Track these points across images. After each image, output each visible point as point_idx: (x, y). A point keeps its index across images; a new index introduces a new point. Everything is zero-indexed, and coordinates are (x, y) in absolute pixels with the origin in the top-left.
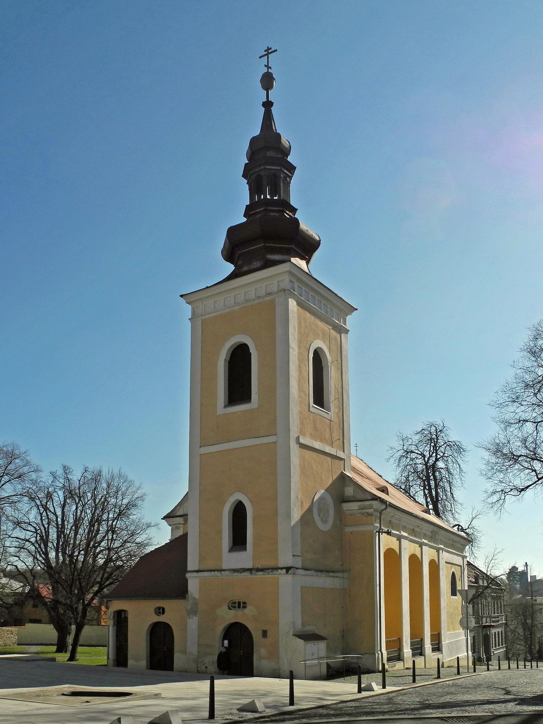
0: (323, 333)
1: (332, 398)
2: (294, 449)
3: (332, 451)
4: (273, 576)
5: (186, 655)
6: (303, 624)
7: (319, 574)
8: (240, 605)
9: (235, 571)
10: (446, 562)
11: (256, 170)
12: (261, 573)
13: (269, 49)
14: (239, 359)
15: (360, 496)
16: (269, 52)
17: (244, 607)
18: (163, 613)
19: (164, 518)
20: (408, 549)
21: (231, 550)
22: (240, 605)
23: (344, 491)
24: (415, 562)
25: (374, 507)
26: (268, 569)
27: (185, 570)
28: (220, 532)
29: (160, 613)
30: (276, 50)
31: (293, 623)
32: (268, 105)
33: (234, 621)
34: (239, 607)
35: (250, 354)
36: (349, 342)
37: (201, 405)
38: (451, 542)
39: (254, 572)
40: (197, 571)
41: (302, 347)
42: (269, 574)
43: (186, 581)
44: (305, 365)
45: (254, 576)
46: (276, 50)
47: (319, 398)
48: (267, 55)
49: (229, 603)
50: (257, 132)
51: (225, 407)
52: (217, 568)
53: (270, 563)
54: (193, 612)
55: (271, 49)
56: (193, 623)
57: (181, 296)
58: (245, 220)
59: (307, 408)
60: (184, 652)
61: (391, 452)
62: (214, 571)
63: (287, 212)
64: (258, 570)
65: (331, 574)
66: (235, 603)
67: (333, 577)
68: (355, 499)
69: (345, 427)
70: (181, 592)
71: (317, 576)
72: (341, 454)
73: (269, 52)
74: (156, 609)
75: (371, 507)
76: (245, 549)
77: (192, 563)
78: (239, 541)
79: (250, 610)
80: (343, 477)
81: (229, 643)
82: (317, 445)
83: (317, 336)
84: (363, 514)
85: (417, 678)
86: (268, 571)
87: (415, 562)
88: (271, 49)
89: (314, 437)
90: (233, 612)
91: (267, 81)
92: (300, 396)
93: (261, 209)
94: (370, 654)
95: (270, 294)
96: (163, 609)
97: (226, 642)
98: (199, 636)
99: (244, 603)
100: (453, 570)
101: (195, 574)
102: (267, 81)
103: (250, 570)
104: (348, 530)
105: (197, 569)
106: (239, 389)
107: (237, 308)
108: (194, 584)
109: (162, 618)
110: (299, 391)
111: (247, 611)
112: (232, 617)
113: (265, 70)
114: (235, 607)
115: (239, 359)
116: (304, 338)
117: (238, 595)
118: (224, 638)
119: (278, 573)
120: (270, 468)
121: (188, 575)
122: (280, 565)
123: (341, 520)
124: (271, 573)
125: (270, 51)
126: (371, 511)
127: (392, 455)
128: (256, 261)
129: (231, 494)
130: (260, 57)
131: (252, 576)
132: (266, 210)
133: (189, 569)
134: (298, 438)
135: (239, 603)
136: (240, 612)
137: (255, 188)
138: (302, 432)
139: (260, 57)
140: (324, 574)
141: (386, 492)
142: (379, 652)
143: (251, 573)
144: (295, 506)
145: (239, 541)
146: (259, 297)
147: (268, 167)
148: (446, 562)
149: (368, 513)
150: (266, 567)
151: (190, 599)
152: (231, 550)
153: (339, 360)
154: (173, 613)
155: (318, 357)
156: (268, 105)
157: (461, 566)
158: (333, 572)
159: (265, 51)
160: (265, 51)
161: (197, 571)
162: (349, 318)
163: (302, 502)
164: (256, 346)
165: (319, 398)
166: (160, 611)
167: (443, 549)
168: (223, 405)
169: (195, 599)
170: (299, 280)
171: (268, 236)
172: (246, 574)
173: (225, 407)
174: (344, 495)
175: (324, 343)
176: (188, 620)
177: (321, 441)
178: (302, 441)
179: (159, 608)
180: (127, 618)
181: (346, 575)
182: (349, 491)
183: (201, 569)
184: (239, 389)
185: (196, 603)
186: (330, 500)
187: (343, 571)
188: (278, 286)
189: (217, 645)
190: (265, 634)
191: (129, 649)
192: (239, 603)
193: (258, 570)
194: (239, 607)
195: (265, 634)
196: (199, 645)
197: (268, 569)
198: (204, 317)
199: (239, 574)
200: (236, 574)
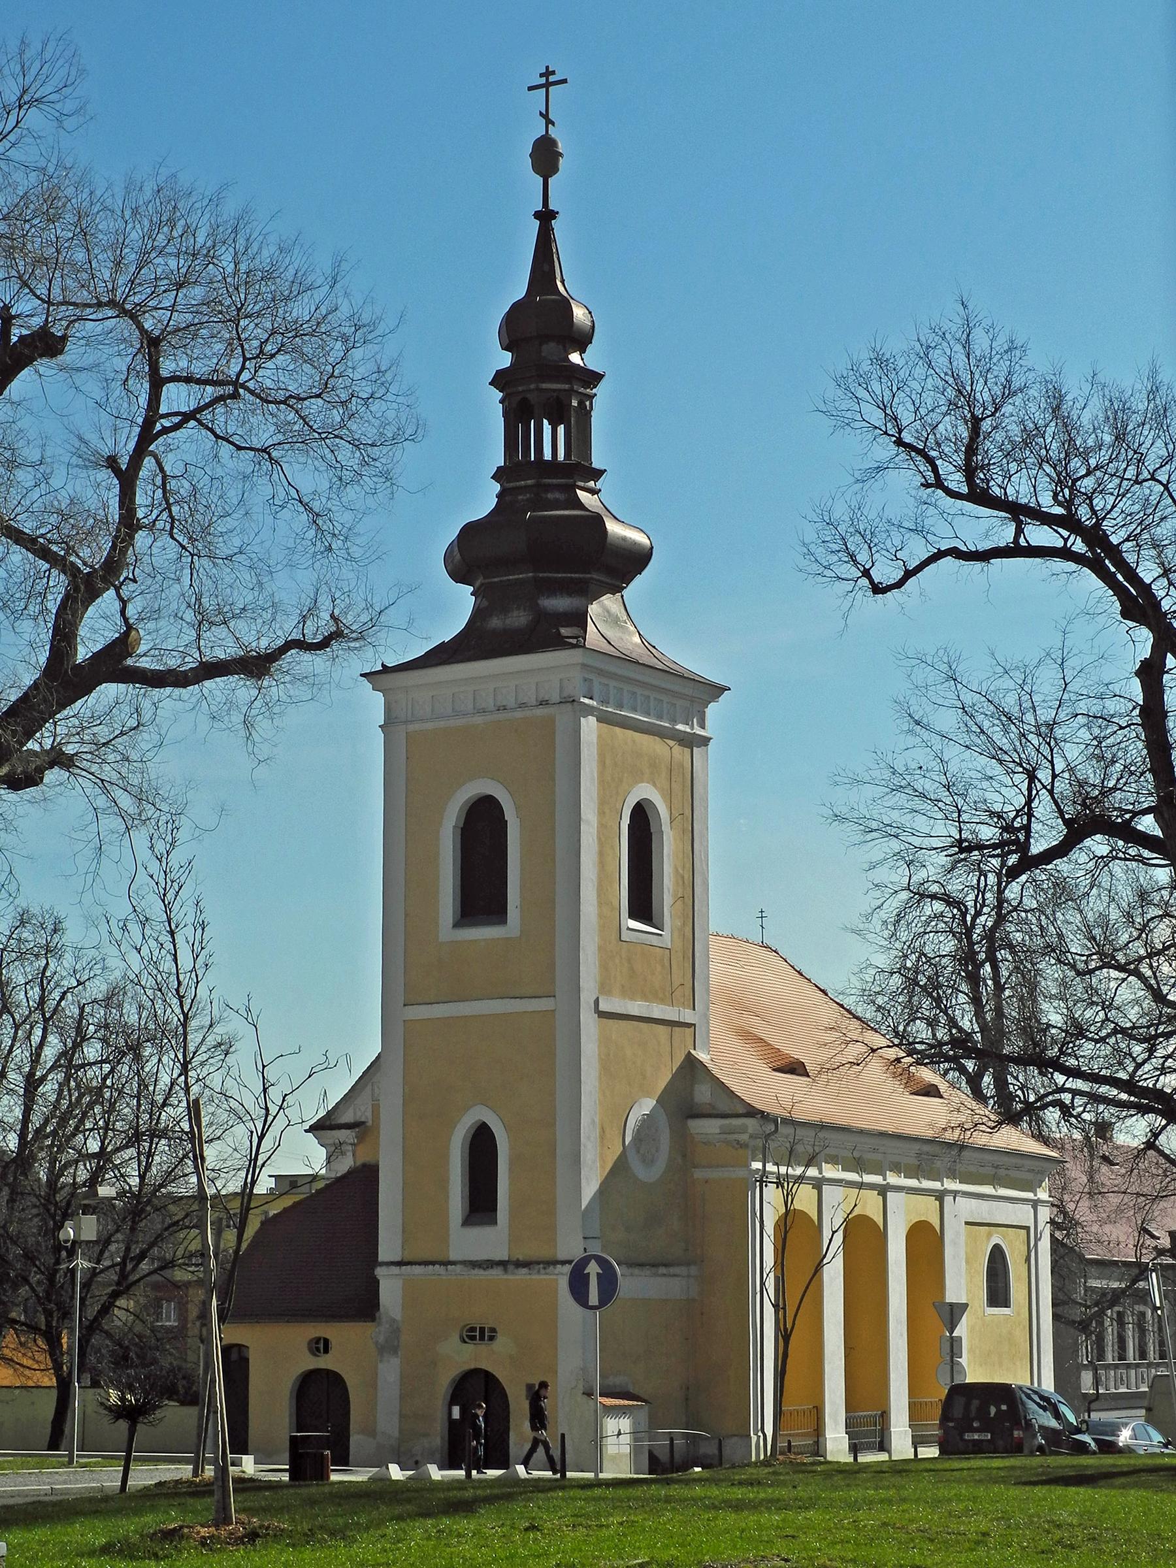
0: (654, 765)
1: (668, 900)
2: (588, 1021)
3: (670, 1013)
4: (548, 1277)
5: (374, 1437)
7: (636, 1271)
8: (477, 1334)
9: (474, 1264)
10: (967, 1223)
11: (520, 389)
12: (525, 1270)
13: (548, 73)
14: (483, 828)
15: (723, 1106)
16: (548, 80)
17: (491, 1338)
18: (326, 1351)
19: (312, 1129)
20: (836, 1208)
21: (467, 1222)
22: (477, 1334)
23: (692, 1096)
24: (864, 1237)
25: (750, 1131)
26: (538, 1263)
27: (371, 1259)
28: (443, 1184)
29: (318, 1349)
30: (564, 81)
31: (584, 1369)
32: (546, 217)
33: (473, 1367)
34: (482, 1338)
36: (712, 766)
37: (406, 915)
38: (991, 1171)
39: (511, 1267)
40: (399, 1264)
41: (607, 811)
42: (539, 1272)
43: (377, 1282)
44: (612, 847)
45: (510, 1277)
46: (564, 81)
47: (642, 905)
48: (547, 85)
49: (462, 1330)
50: (520, 292)
51: (457, 925)
52: (440, 1258)
53: (544, 1253)
54: (389, 1347)
55: (553, 73)
56: (390, 1371)
59: (615, 935)
60: (371, 1432)
61: (878, 894)
62: (433, 1263)
63: (581, 484)
64: (519, 1264)
65: (662, 1270)
66: (473, 1329)
67: (664, 1275)
68: (715, 1112)
69: (697, 954)
70: (365, 1306)
71: (632, 1275)
72: (688, 1016)
73: (548, 80)
74: (311, 1341)
75: (743, 1129)
76: (494, 1222)
77: (388, 1248)
78: (481, 1204)
79: (502, 1344)
80: (691, 1065)
81: (462, 1412)
82: (636, 1007)
83: (637, 776)
84: (727, 1143)
86: (537, 1267)
88: (553, 73)
89: (629, 993)
90: (470, 1348)
91: (545, 157)
92: (601, 916)
93: (529, 482)
94: (741, 1436)
95: (543, 703)
96: (326, 1341)
97: (456, 1412)
98: (402, 1397)
99: (493, 1330)
100: (995, 1240)
101: (395, 1270)
102: (545, 157)
103: (503, 1264)
104: (698, 1174)
105: (398, 1259)
106: (482, 897)
107: (478, 720)
108: (391, 1290)
109: (324, 1362)
110: (600, 904)
112: (465, 1356)
114: (473, 1338)
115: (483, 828)
116: (615, 775)
117: (479, 1315)
118: (452, 1403)
119: (556, 1272)
120: (545, 1055)
121: (380, 1272)
122: (561, 1256)
123: (684, 1156)
124: (542, 1271)
125: (552, 79)
126: (744, 1137)
127: (879, 902)
128: (518, 609)
129: (467, 1108)
130: (530, 89)
131: (505, 1277)
132: (538, 485)
133: (380, 1259)
134: (597, 1002)
135: (482, 1330)
137: (519, 414)
138: (605, 988)
139: (530, 89)
140: (647, 1271)
141: (800, 1071)
142: (760, 1434)
143: (506, 1270)
144: (589, 1138)
145: (481, 1204)
146: (522, 706)
147: (544, 386)
148: (967, 1223)
149: (738, 1142)
150: (534, 1259)
151: (384, 1320)
152: (467, 1222)
153: (688, 812)
154: (349, 1348)
155: (641, 817)
156: (546, 217)
157: (1027, 1228)
158: (665, 1265)
159: (541, 75)
160: (541, 75)
161: (399, 1264)
162: (712, 710)
163: (603, 1130)
164: (518, 808)
165: (642, 905)
166: (321, 1346)
167: (955, 1193)
168: (450, 921)
169: (394, 1320)
170: (601, 673)
171: (541, 559)
172: (496, 1272)
173: (457, 925)
174: (692, 1099)
175: (655, 785)
176: (380, 1366)
177: (645, 998)
178: (603, 1007)
179: (318, 1340)
180: (247, 1360)
181: (694, 1270)
182: (703, 1094)
183: (406, 1260)
184: (482, 897)
185: (396, 1331)
186: (663, 1121)
187: (688, 1264)
188: (561, 688)
189: (439, 1412)
191: (250, 1424)
192: (482, 1330)
193: (519, 1264)
194: (482, 1338)
196: (402, 1416)
197: (538, 1263)
198: (411, 727)
199: (481, 1272)
200: (476, 1271)
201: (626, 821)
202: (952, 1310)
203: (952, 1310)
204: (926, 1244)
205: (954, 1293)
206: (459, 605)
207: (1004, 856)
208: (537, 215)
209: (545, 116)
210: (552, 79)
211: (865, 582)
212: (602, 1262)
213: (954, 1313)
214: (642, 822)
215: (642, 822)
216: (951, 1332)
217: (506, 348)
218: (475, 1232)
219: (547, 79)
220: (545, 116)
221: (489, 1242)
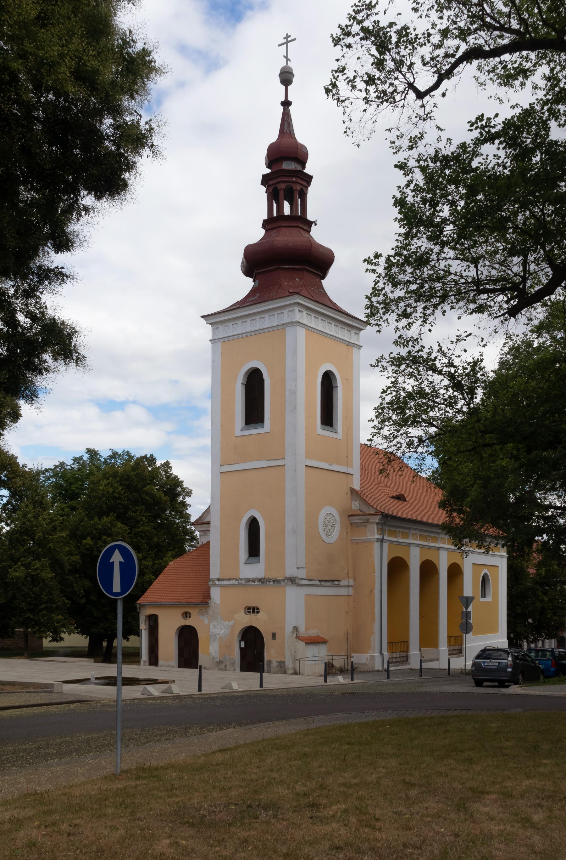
6: (307, 629)
8: (253, 610)
13: (288, 36)
17: (258, 612)
18: (190, 617)
24: (428, 570)
29: (186, 617)
30: (295, 39)
32: (286, 104)
33: (249, 625)
35: (263, 380)
46: (295, 39)
47: (328, 418)
48: (287, 43)
55: (290, 36)
57: (202, 317)
58: (269, 171)
66: (250, 608)
73: (288, 40)
78: (254, 551)
79: (262, 615)
85: (390, 675)
87: (428, 570)
88: (290, 36)
91: (286, 78)
96: (190, 613)
100: (485, 571)
102: (286, 78)
106: (254, 413)
109: (188, 622)
111: (259, 616)
112: (247, 620)
113: (284, 64)
114: (250, 612)
115: (254, 383)
125: (289, 39)
130: (280, 45)
136: (252, 616)
139: (280, 45)
145: (254, 551)
156: (286, 104)
159: (284, 38)
160: (284, 38)
165: (328, 418)
179: (186, 613)
184: (254, 413)
190: (274, 635)
192: (253, 609)
195: (274, 635)
201: (319, 379)
202: (467, 614)
203: (467, 614)
204: (455, 572)
205: (468, 591)
206: (248, 284)
207: (461, 521)
208: (283, 104)
209: (286, 57)
210: (289, 39)
211: (411, 93)
212: (124, 552)
213: (467, 601)
214: (328, 381)
215: (328, 381)
216: (467, 608)
217: (269, 166)
218: (249, 567)
219: (287, 40)
220: (286, 57)
221: (255, 571)
